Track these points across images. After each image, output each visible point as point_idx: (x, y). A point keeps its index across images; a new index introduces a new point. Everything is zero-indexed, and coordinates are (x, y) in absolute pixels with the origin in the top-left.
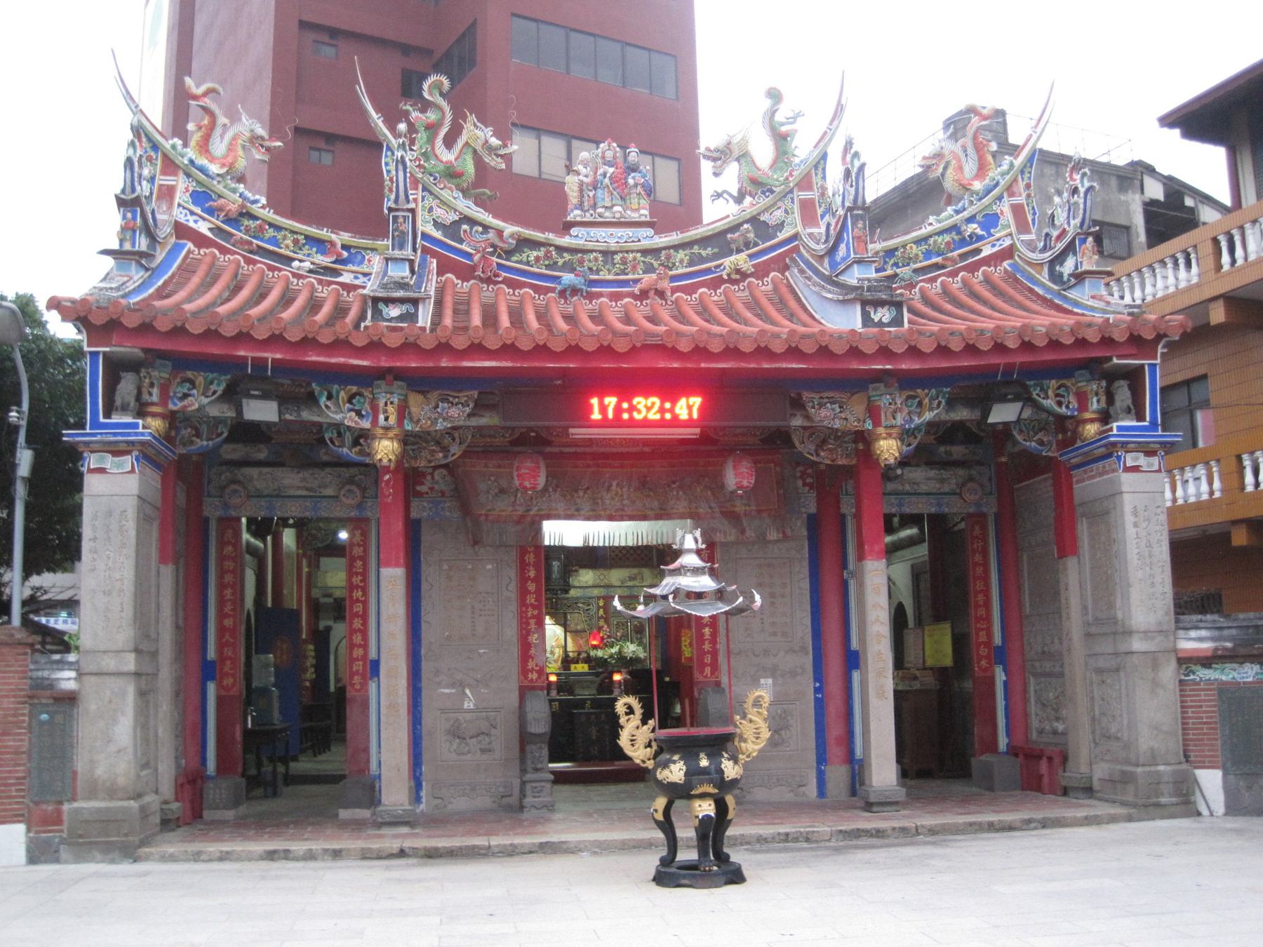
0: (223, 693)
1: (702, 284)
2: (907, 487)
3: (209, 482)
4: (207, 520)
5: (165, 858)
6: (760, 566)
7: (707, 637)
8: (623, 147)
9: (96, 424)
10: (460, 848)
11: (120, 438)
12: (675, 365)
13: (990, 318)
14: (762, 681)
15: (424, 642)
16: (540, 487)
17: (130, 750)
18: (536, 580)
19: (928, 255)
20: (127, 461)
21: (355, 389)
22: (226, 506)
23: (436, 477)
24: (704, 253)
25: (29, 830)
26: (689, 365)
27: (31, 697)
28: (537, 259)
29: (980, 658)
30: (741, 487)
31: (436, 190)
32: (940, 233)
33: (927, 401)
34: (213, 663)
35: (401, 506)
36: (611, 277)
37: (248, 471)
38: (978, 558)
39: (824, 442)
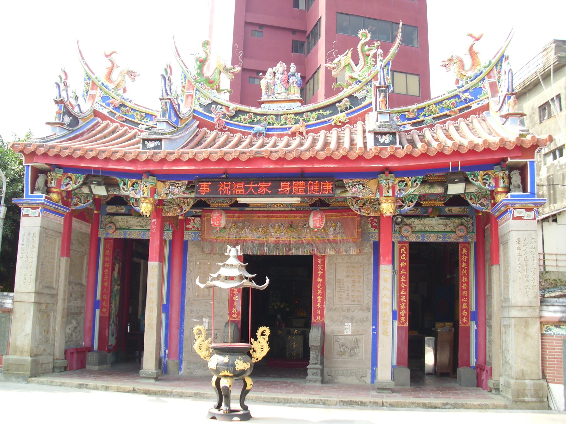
0: (400, 325)
2: (427, 228)
3: (102, 222)
5: (39, 383)
6: (348, 267)
7: (319, 301)
8: (288, 65)
9: (28, 196)
10: (159, 391)
11: (33, 202)
12: (271, 167)
14: (346, 324)
15: (187, 297)
16: (222, 226)
17: (30, 336)
19: (442, 110)
21: (134, 180)
23: (195, 221)
24: (325, 113)
26: (278, 167)
28: (245, 119)
29: (463, 317)
30: (316, 227)
31: (201, 90)
32: (448, 99)
33: (410, 183)
34: (99, 301)
35: (158, 233)
36: (279, 126)
38: (464, 265)
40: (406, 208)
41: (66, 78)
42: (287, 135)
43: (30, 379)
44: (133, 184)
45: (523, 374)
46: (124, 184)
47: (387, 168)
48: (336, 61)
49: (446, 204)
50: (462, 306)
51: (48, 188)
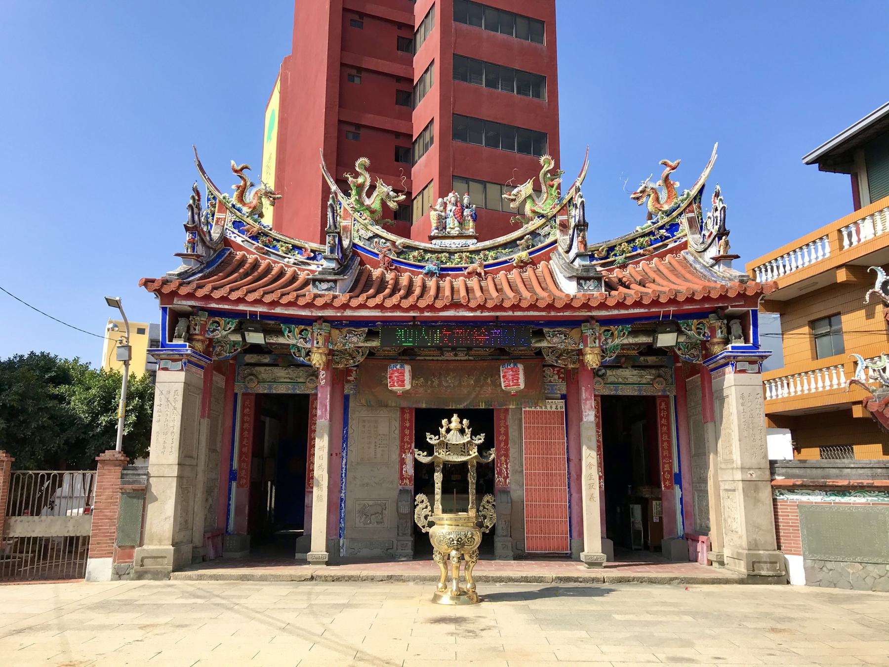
1: (502, 269)
2: (620, 380)
4: (236, 394)
13: (686, 280)
17: (172, 519)
18: (410, 428)
20: (179, 365)
21: (303, 327)
22: (246, 387)
25: (114, 561)
27: (121, 489)
37: (257, 368)
38: (664, 421)
39: (561, 355)
40: (608, 359)
41: (199, 200)
42: (463, 275)
43: (172, 574)
44: (302, 331)
45: (756, 545)
46: (290, 332)
47: (592, 317)
48: (515, 191)
49: (641, 354)
50: (663, 468)
51: (190, 335)
